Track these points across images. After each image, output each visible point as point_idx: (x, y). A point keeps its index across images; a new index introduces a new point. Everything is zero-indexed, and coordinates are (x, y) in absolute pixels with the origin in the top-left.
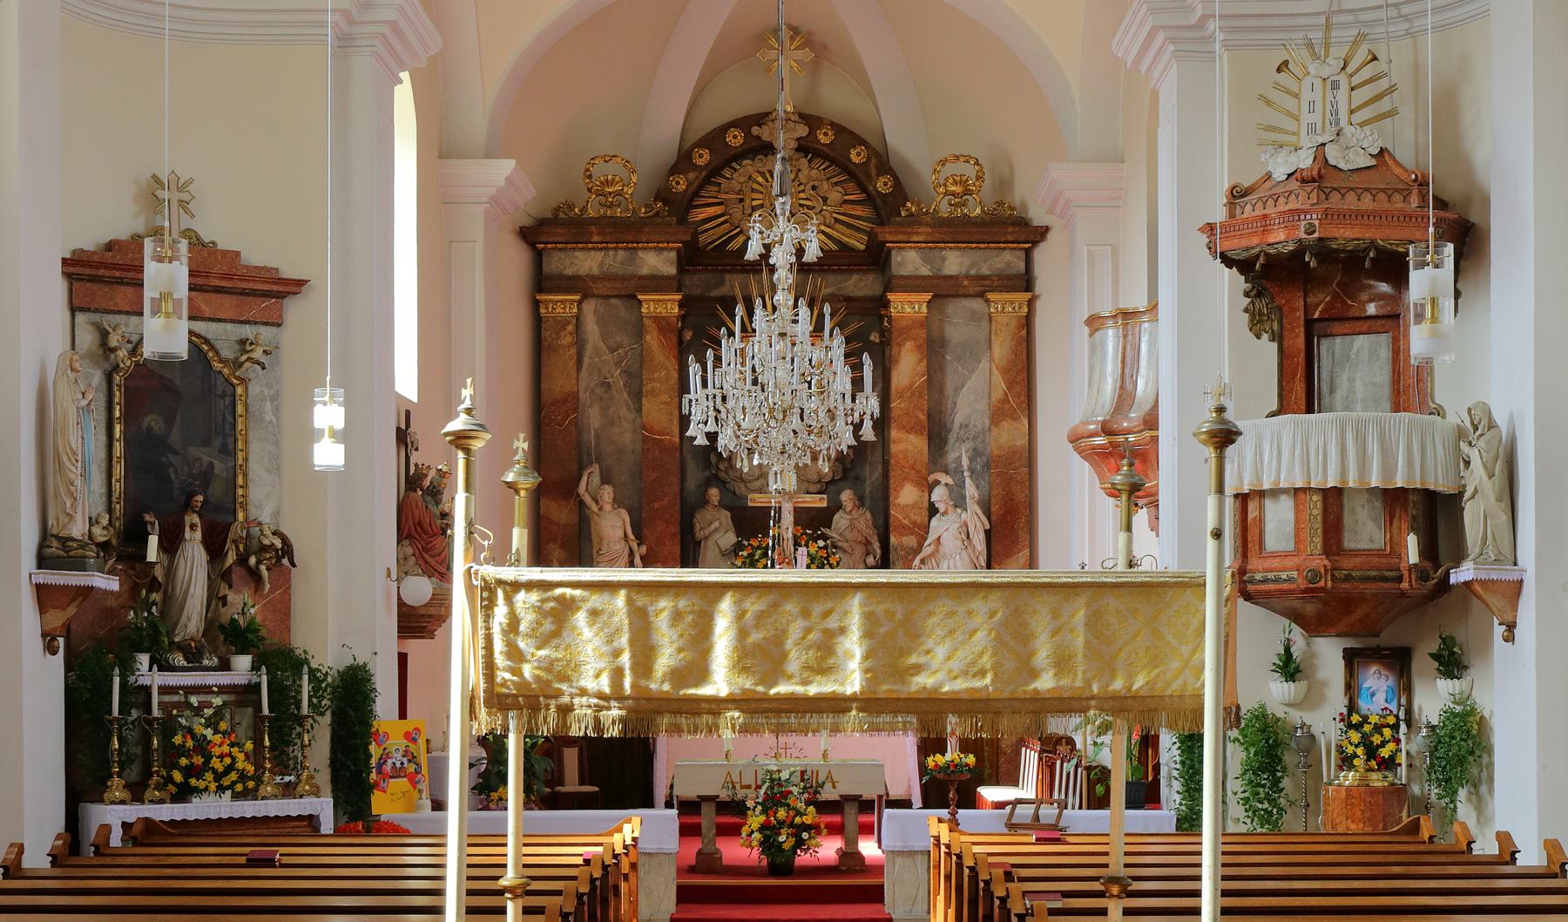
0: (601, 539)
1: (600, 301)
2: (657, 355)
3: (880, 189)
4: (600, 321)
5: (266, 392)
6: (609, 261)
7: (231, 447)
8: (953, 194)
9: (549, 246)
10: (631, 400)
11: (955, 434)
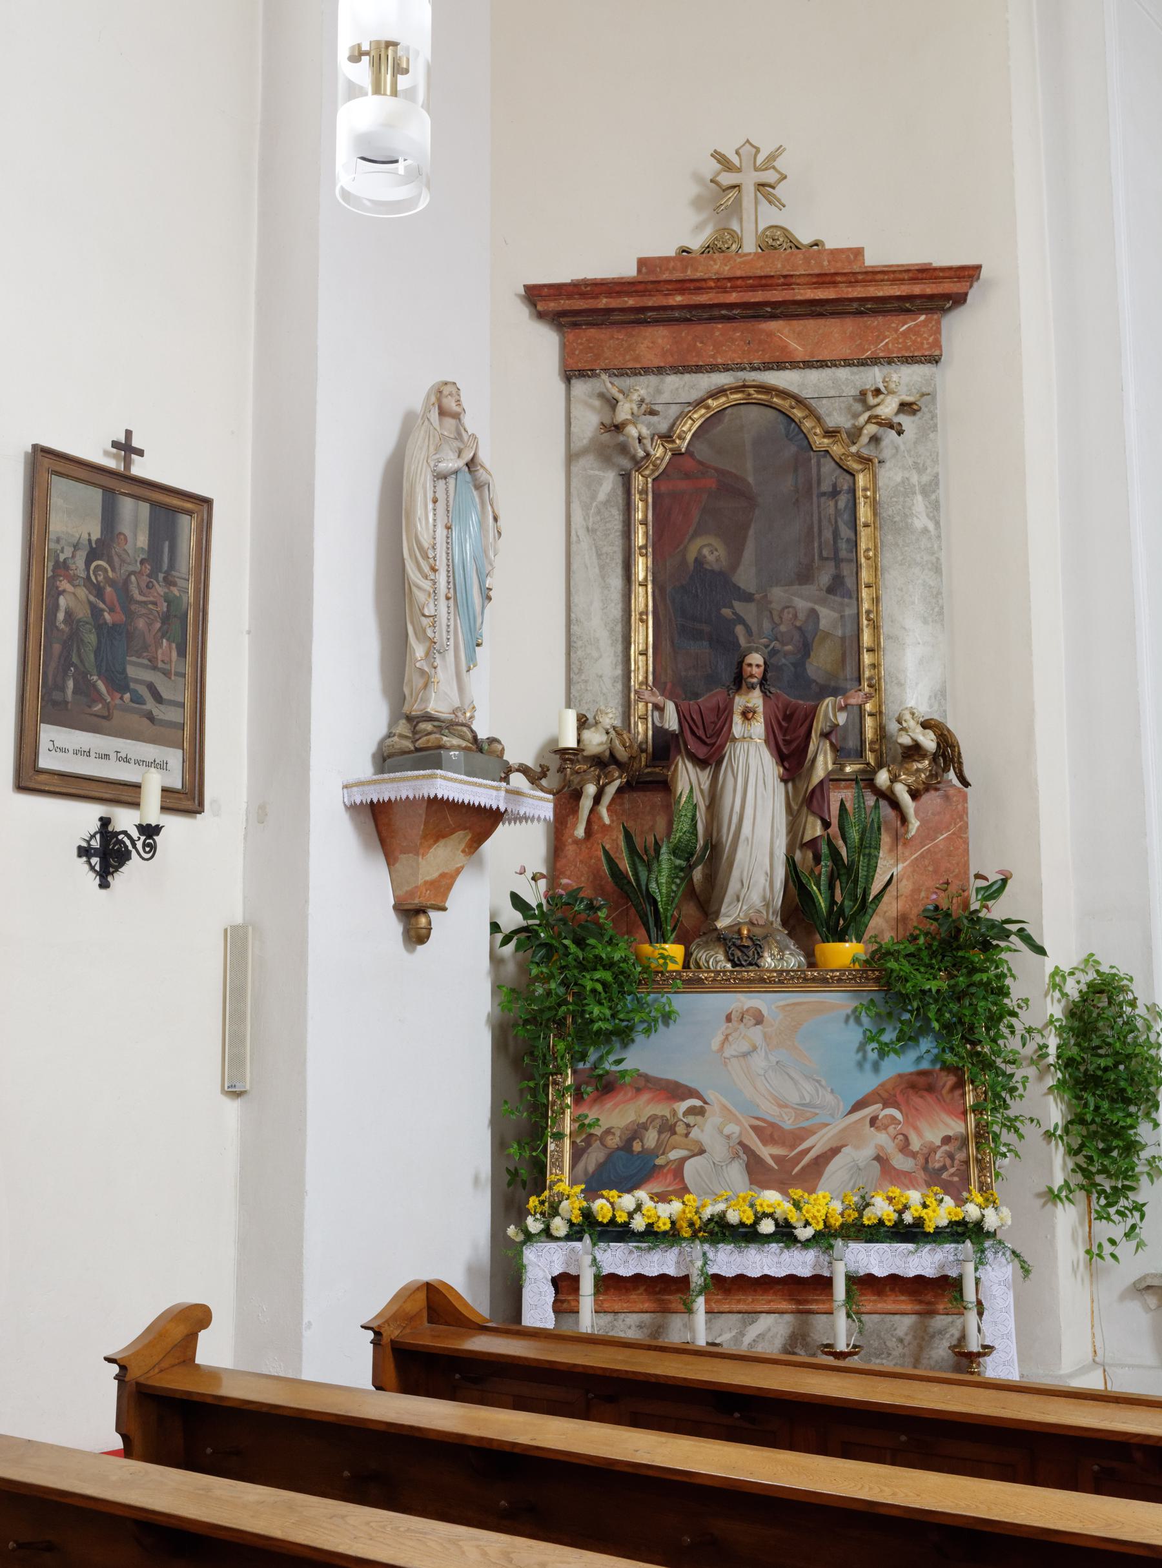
5: (915, 479)
7: (849, 582)
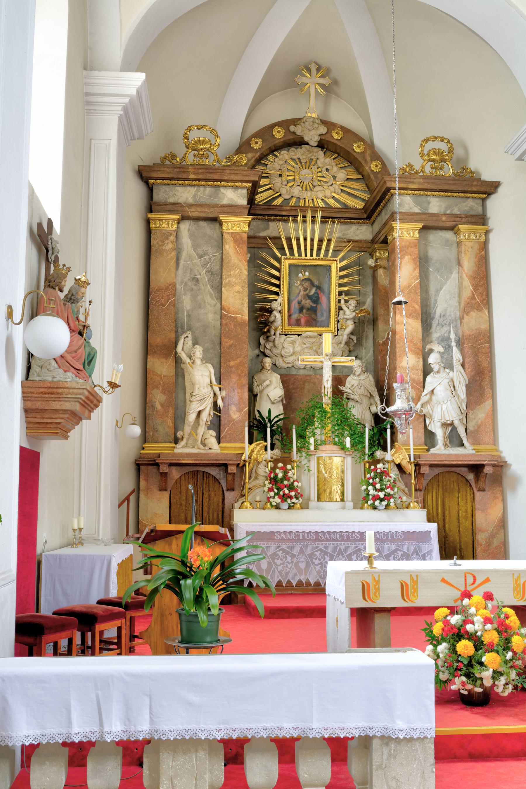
0: (193, 385)
1: (192, 222)
2: (233, 259)
3: (372, 169)
4: (192, 236)
6: (200, 194)
8: (434, 161)
9: (158, 181)
10: (213, 290)
11: (437, 321)
